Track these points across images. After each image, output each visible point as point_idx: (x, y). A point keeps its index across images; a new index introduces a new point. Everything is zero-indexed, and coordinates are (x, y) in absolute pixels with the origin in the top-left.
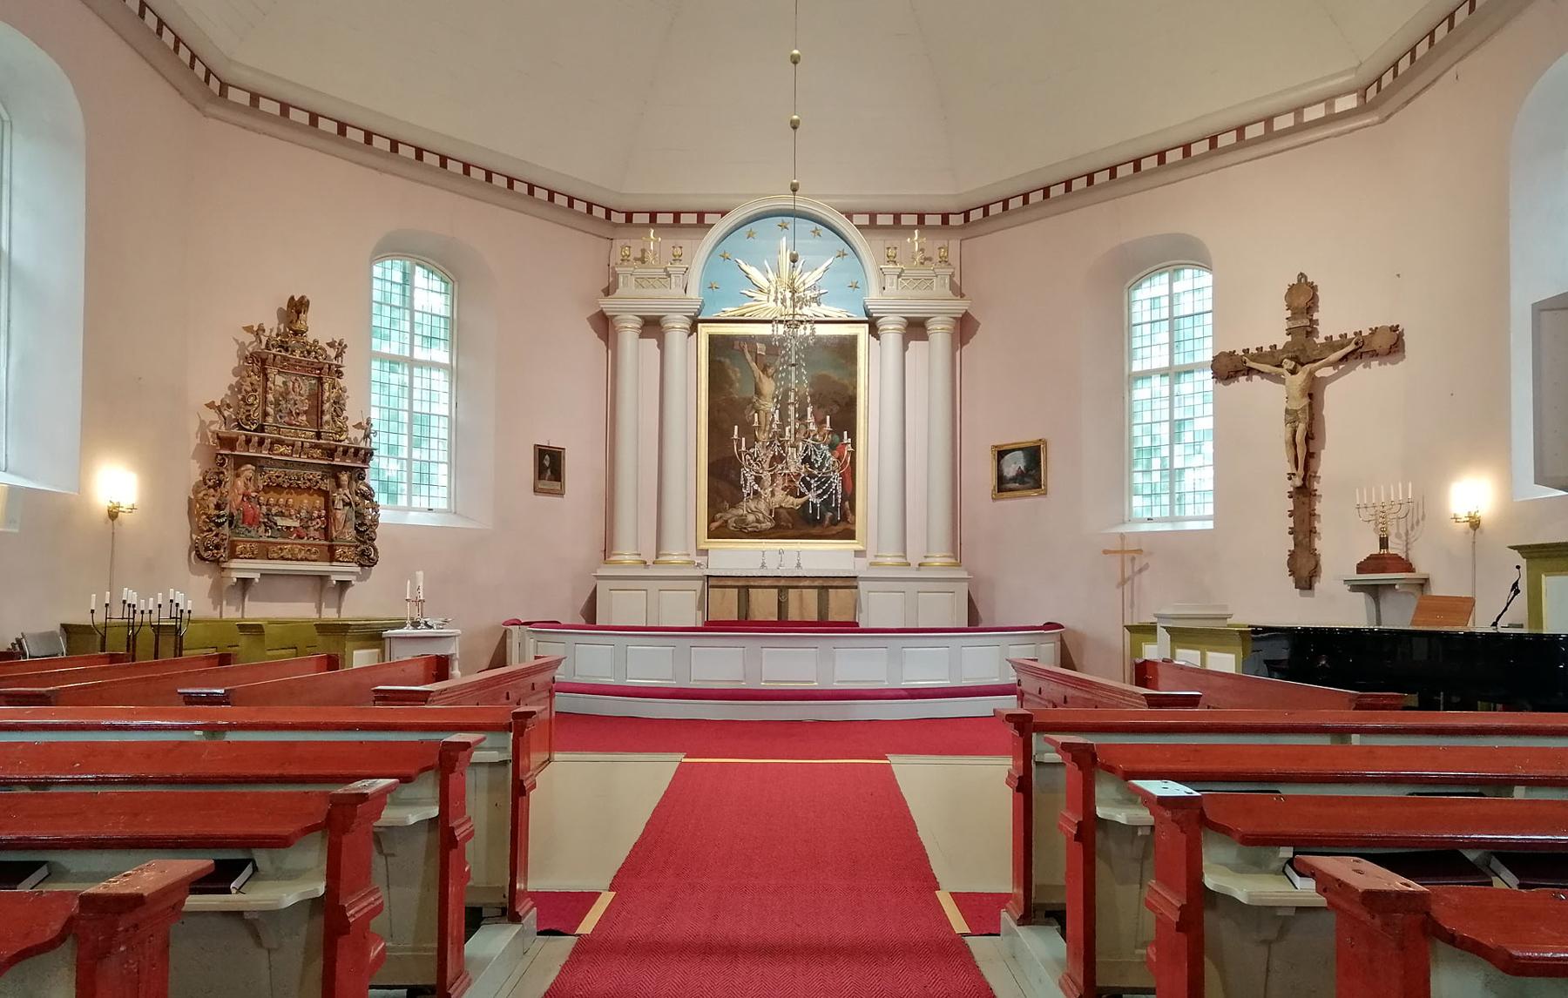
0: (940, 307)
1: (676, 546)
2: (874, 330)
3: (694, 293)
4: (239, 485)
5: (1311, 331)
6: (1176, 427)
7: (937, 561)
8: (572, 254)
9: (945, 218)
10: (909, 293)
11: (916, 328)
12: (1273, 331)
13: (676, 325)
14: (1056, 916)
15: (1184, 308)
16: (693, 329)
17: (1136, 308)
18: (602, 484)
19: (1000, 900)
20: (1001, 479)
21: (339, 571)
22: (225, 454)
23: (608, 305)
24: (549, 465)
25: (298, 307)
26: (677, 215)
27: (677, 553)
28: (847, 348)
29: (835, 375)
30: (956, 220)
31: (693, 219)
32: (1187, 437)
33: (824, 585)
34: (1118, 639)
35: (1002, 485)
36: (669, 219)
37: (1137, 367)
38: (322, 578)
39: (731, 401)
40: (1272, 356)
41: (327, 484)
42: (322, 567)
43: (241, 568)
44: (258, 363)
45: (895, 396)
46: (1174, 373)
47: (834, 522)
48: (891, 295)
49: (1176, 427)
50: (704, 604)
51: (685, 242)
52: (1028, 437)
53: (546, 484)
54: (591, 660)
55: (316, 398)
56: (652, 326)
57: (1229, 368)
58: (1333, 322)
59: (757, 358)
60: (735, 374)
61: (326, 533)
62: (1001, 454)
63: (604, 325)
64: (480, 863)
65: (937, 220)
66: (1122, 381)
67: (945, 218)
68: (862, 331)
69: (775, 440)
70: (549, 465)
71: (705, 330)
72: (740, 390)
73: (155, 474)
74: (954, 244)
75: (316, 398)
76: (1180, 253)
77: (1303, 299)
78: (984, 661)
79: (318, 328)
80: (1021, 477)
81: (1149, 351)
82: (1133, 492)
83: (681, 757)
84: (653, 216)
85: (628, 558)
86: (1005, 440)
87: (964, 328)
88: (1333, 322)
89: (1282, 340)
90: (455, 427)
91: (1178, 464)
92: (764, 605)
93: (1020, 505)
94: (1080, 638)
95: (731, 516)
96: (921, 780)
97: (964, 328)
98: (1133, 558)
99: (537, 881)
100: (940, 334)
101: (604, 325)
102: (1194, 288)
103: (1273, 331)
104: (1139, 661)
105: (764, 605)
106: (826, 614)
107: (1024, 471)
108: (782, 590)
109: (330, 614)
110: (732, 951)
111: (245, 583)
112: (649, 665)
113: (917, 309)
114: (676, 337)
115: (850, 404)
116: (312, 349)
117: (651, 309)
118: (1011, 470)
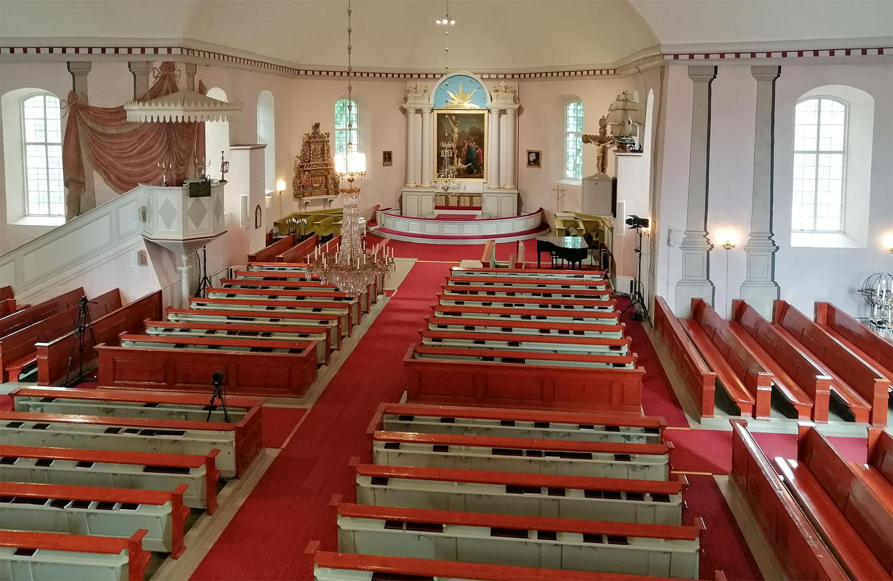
0: (511, 107)
1: (427, 182)
2: (489, 111)
3: (432, 102)
4: (304, 177)
7: (509, 187)
8: (391, 91)
11: (503, 112)
12: (596, 132)
13: (427, 111)
16: (432, 110)
18: (404, 154)
20: (529, 161)
21: (329, 197)
22: (301, 170)
23: (405, 106)
24: (388, 157)
25: (317, 126)
26: (427, 75)
29: (477, 126)
31: (432, 76)
33: (471, 196)
37: (568, 130)
38: (326, 200)
40: (594, 138)
41: (326, 173)
42: (325, 197)
43: (306, 199)
44: (308, 143)
47: (477, 173)
50: (435, 200)
51: (429, 84)
53: (387, 163)
54: (400, 225)
55: (323, 150)
56: (419, 111)
57: (586, 139)
60: (446, 126)
61: (326, 187)
62: (529, 153)
63: (404, 111)
64: (379, 287)
65: (510, 76)
68: (486, 112)
70: (388, 157)
71: (436, 112)
73: (286, 180)
74: (517, 83)
75: (323, 150)
76: (577, 99)
79: (322, 130)
83: (416, 260)
84: (419, 75)
87: (519, 111)
89: (598, 135)
92: (453, 202)
93: (533, 170)
97: (519, 111)
99: (385, 289)
101: (404, 111)
103: (596, 132)
105: (453, 202)
106: (468, 208)
107: (535, 160)
109: (327, 208)
110: (412, 299)
111: (307, 203)
112: (415, 227)
113: (503, 107)
114: (427, 115)
115: (482, 135)
116: (322, 136)
117: (419, 107)
118: (532, 159)
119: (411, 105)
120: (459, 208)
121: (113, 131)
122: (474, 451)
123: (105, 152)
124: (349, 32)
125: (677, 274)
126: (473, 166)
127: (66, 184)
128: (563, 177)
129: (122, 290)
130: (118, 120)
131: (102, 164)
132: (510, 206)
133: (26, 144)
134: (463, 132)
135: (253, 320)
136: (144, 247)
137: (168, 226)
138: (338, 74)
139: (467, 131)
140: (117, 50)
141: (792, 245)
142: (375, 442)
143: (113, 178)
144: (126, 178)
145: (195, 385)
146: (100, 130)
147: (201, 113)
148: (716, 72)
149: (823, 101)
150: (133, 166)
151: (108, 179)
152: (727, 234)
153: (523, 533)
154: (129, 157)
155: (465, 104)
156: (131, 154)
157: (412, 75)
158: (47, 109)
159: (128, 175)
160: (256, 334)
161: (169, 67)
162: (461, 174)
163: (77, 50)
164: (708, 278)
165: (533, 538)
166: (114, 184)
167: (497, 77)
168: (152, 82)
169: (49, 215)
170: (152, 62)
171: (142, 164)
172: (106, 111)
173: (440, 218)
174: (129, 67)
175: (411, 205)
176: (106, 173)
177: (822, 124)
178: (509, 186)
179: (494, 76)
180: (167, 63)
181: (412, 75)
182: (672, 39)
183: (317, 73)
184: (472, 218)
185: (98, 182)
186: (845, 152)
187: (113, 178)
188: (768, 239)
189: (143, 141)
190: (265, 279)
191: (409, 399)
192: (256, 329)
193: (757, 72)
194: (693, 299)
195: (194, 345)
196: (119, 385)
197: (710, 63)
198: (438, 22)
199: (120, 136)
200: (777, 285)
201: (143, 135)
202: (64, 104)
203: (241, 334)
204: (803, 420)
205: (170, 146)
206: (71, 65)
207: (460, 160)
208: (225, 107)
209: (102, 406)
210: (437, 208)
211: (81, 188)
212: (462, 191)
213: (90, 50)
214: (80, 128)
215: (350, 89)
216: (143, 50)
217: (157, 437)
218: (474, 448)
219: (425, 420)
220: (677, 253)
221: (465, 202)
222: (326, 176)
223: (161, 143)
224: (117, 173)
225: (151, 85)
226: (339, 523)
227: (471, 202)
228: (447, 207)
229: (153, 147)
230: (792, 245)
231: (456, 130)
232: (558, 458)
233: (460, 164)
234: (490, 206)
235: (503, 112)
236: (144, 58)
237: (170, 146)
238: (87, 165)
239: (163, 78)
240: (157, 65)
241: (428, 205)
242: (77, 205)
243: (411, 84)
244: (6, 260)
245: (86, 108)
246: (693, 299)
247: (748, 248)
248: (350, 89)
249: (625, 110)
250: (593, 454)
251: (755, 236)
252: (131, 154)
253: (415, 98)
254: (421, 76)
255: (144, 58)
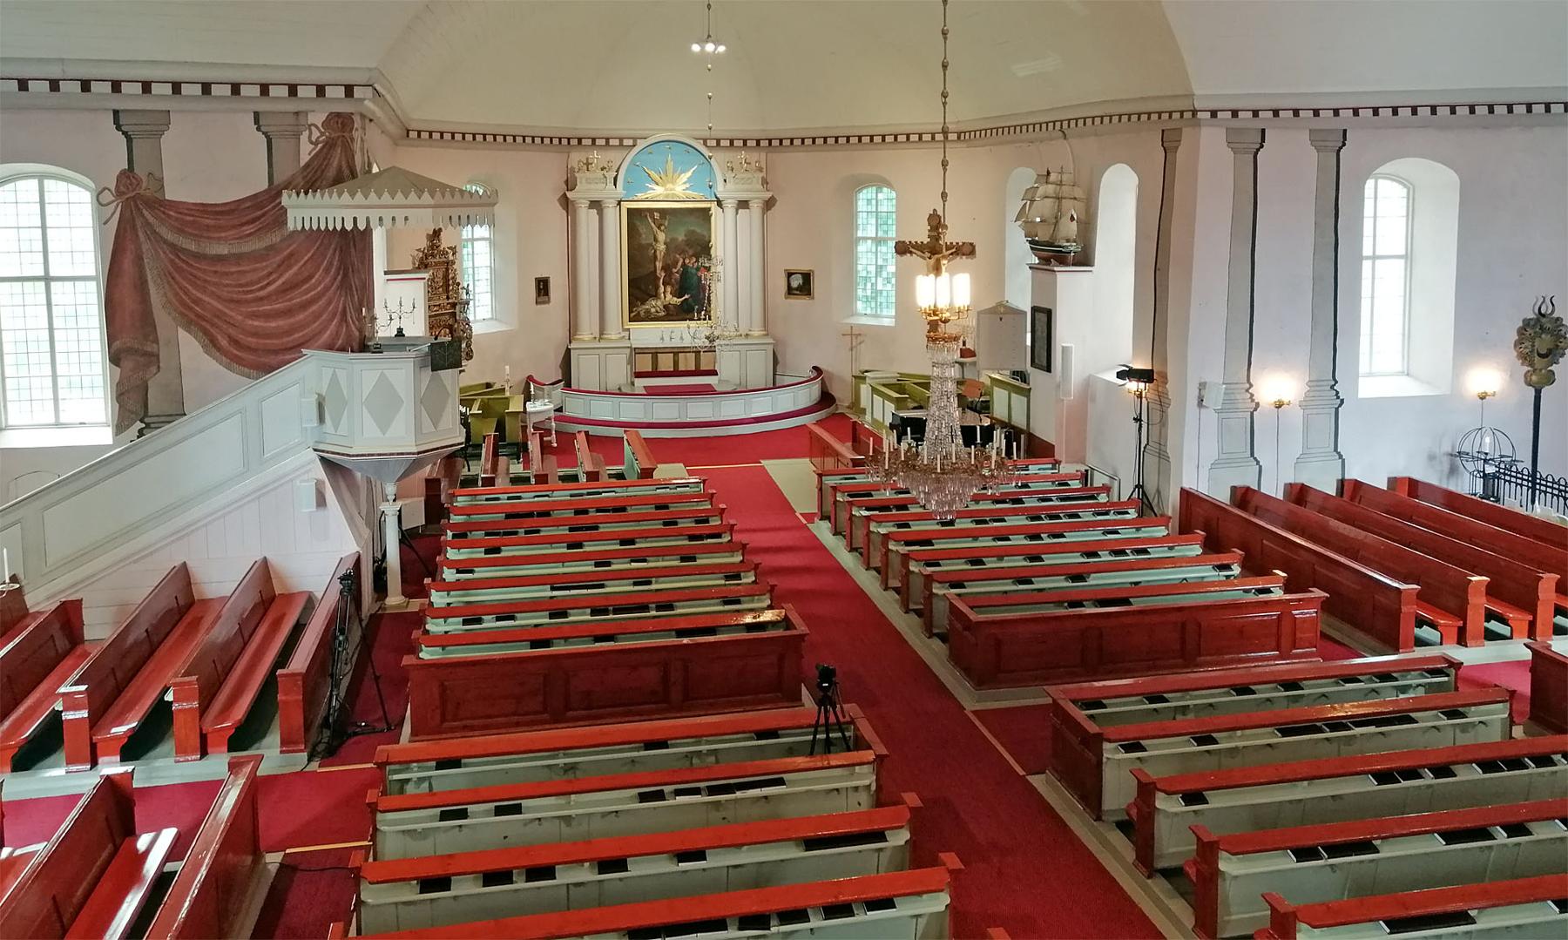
0: (757, 196)
2: (719, 203)
5: (937, 238)
6: (879, 269)
7: (756, 333)
8: (547, 169)
9: (758, 142)
10: (740, 186)
11: (743, 204)
12: (922, 235)
14: (828, 518)
15: (883, 208)
17: (860, 203)
19: (813, 514)
24: (543, 287)
25: (437, 233)
26: (594, 140)
27: (613, 332)
28: (705, 214)
30: (764, 143)
32: (884, 274)
34: (849, 378)
35: (790, 291)
36: (603, 142)
37: (860, 234)
39: (641, 246)
40: (920, 247)
45: (734, 251)
46: (878, 241)
48: (729, 191)
49: (879, 269)
52: (805, 268)
55: (446, 277)
56: (596, 205)
57: (902, 249)
58: (950, 237)
59: (654, 220)
60: (642, 229)
62: (790, 274)
65: (754, 143)
66: (853, 241)
67: (758, 142)
68: (714, 206)
69: (667, 272)
70: (543, 287)
72: (645, 239)
74: (763, 155)
75: (446, 277)
76: (880, 182)
77: (936, 223)
78: (786, 400)
79: (445, 242)
80: (799, 288)
81: (866, 227)
82: (857, 299)
85: (586, 337)
86: (792, 268)
87: (769, 204)
88: (950, 237)
89: (926, 240)
90: (493, 271)
91: (880, 287)
92: (666, 363)
93: (800, 302)
94: (831, 376)
95: (642, 309)
96: (777, 469)
97: (769, 204)
98: (856, 336)
100: (756, 207)
101: (566, 203)
102: (886, 199)
103: (922, 235)
104: (810, 912)
105: (666, 363)
107: (802, 285)
108: (676, 354)
113: (744, 196)
116: (445, 253)
118: (795, 284)
119: (580, 195)
120: (676, 373)
121: (223, 249)
122: (1248, 738)
123: (204, 291)
124: (945, 67)
125: (1210, 451)
126: (692, 300)
127: (115, 358)
128: (854, 314)
129: (274, 560)
130: (234, 227)
131: (198, 315)
132: (759, 368)
133: (1405, 257)
134: (673, 240)
135: (602, 586)
136: (320, 472)
137: (384, 425)
138: (819, 141)
139: (681, 237)
140: (206, 88)
141: (1361, 395)
142: (379, 816)
143: (224, 342)
144: (252, 341)
145: (476, 722)
146: (192, 247)
147: (368, 212)
148: (1263, 140)
149: (46, 182)
150: (268, 316)
151: (211, 344)
152: (1279, 384)
153: (1483, 833)
154: (261, 299)
155: (673, 189)
156: (262, 293)
157: (580, 140)
158: (48, 208)
159: (255, 335)
160: (645, 608)
161: (341, 123)
162: (672, 314)
163: (146, 87)
164: (1252, 454)
165: (1501, 836)
166: (225, 353)
167: (621, 144)
168: (306, 152)
169: (58, 425)
170: (306, 113)
171: (288, 312)
172: (204, 209)
173: (652, 392)
174: (257, 121)
175: (585, 371)
176: (206, 332)
177: (1400, 214)
178: (757, 332)
179: (616, 142)
180: (338, 115)
181: (580, 140)
182: (1207, 88)
183: (866, 140)
184: (707, 391)
185: (189, 350)
186: (1409, 257)
187: (224, 342)
188: (1330, 391)
189: (290, 267)
190: (508, 516)
191: (415, 733)
192: (644, 600)
193: (1317, 138)
194: (1234, 489)
195: (566, 639)
196: (452, 730)
197: (1338, 124)
198: (696, 48)
199: (238, 258)
200: (1341, 457)
201: (291, 255)
202: (107, 197)
203: (616, 611)
204: (110, 764)
205: (345, 275)
206: (119, 120)
207: (669, 289)
208: (475, 200)
209: (561, 761)
210: (639, 375)
211: (148, 365)
212: (676, 343)
213: (176, 87)
214: (146, 246)
215: (944, 164)
216: (293, 90)
217: (739, 794)
218: (1248, 732)
219: (1125, 704)
220: (1210, 417)
221: (687, 362)
222: (451, 327)
223: (327, 271)
224: (231, 331)
225: (305, 158)
226: (1222, 866)
227: (676, 363)
228: (655, 373)
229: (311, 277)
230: (1361, 395)
231: (661, 236)
232: (1372, 729)
233: (669, 296)
234: (729, 367)
235: (743, 204)
236: (292, 106)
237: (345, 275)
238: (162, 317)
239: (330, 145)
240: (318, 118)
241: (618, 372)
242: (142, 401)
243: (576, 157)
244: (11, 518)
245: (160, 205)
246: (1234, 489)
247: (1304, 405)
248: (944, 164)
249: (1059, 198)
250: (470, 808)
251: (1313, 384)
252: (262, 293)
253: (588, 181)
254: (584, 142)
255: (292, 106)
